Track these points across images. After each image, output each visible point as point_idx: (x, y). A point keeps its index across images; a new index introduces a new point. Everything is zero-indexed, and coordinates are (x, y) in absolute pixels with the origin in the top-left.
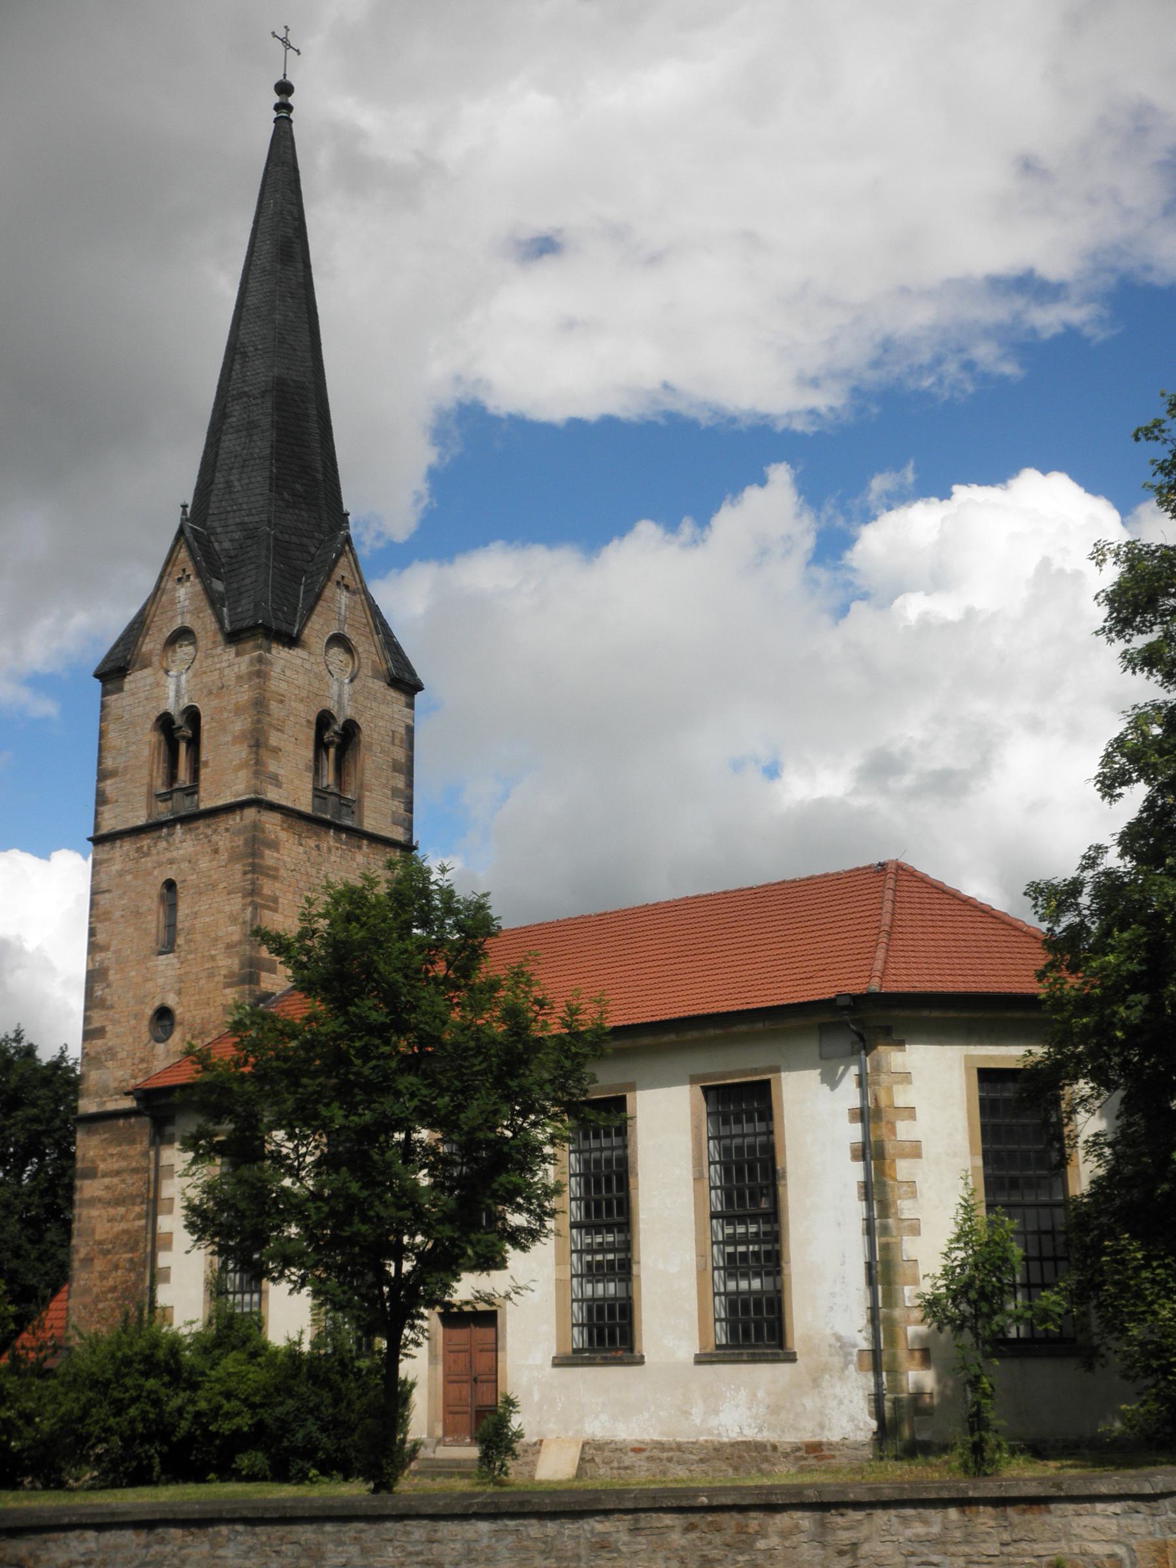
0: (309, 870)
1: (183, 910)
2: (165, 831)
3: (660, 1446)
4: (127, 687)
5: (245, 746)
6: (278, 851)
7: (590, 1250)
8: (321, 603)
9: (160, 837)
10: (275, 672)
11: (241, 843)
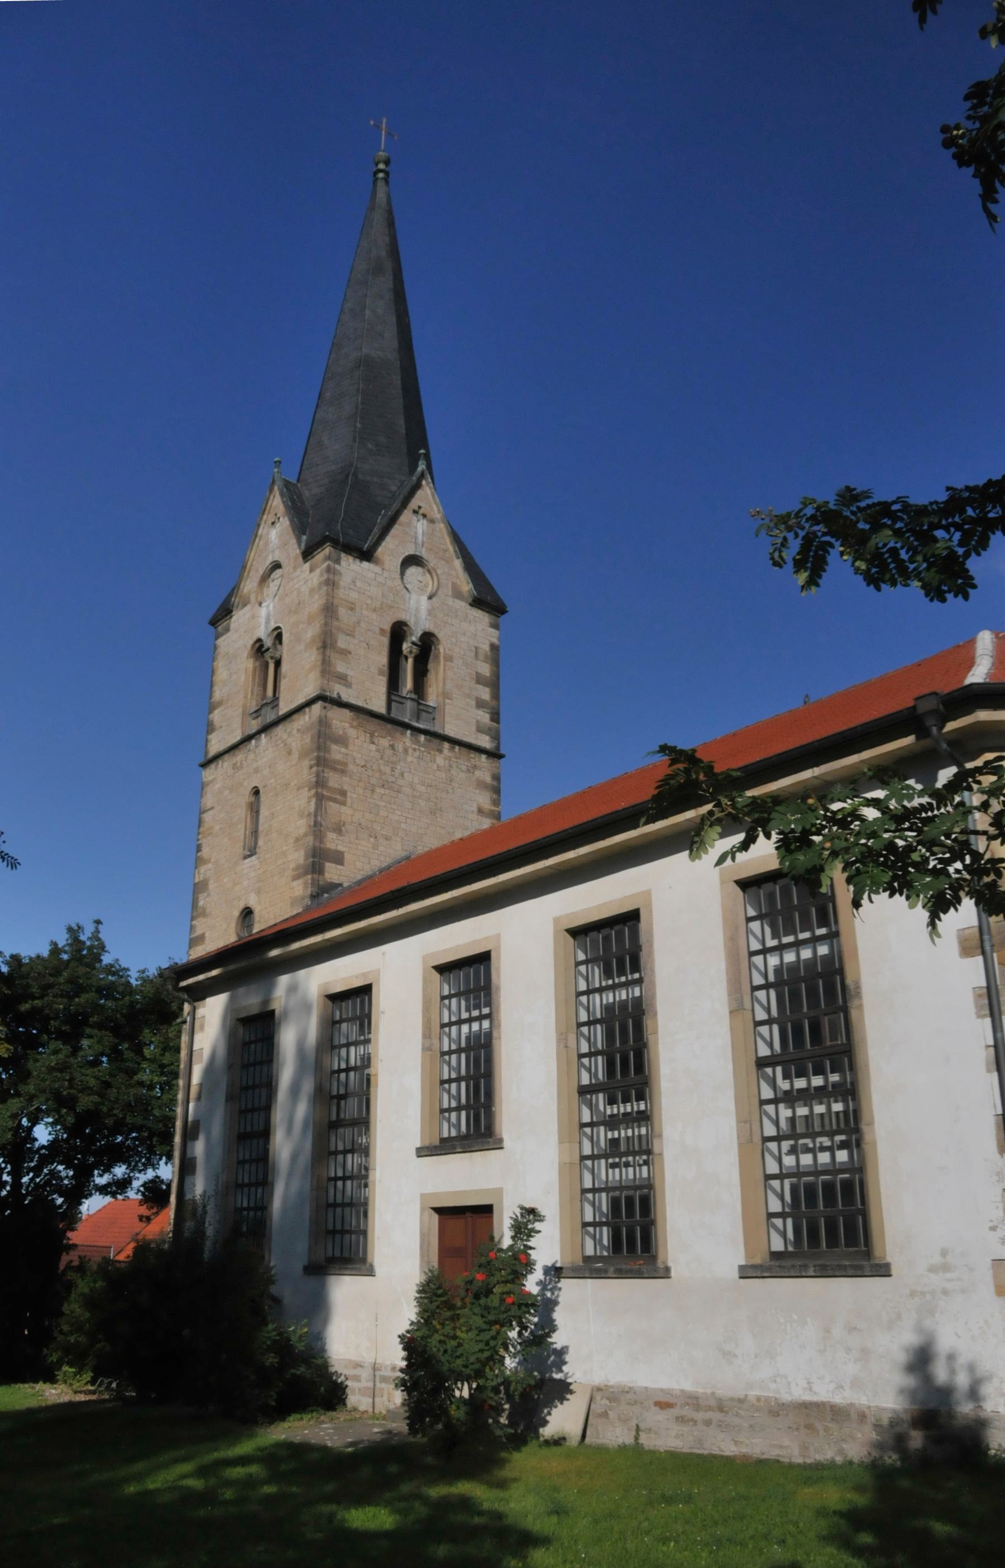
0: (382, 767)
1: (264, 812)
2: (253, 742)
3: (693, 1401)
4: (232, 626)
5: (315, 649)
6: (346, 746)
7: (612, 1123)
8: (396, 526)
9: (249, 751)
10: (345, 581)
11: (308, 740)
